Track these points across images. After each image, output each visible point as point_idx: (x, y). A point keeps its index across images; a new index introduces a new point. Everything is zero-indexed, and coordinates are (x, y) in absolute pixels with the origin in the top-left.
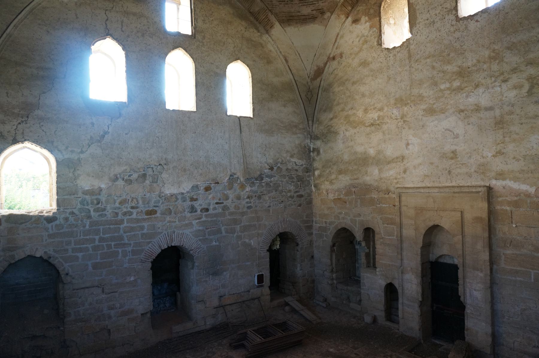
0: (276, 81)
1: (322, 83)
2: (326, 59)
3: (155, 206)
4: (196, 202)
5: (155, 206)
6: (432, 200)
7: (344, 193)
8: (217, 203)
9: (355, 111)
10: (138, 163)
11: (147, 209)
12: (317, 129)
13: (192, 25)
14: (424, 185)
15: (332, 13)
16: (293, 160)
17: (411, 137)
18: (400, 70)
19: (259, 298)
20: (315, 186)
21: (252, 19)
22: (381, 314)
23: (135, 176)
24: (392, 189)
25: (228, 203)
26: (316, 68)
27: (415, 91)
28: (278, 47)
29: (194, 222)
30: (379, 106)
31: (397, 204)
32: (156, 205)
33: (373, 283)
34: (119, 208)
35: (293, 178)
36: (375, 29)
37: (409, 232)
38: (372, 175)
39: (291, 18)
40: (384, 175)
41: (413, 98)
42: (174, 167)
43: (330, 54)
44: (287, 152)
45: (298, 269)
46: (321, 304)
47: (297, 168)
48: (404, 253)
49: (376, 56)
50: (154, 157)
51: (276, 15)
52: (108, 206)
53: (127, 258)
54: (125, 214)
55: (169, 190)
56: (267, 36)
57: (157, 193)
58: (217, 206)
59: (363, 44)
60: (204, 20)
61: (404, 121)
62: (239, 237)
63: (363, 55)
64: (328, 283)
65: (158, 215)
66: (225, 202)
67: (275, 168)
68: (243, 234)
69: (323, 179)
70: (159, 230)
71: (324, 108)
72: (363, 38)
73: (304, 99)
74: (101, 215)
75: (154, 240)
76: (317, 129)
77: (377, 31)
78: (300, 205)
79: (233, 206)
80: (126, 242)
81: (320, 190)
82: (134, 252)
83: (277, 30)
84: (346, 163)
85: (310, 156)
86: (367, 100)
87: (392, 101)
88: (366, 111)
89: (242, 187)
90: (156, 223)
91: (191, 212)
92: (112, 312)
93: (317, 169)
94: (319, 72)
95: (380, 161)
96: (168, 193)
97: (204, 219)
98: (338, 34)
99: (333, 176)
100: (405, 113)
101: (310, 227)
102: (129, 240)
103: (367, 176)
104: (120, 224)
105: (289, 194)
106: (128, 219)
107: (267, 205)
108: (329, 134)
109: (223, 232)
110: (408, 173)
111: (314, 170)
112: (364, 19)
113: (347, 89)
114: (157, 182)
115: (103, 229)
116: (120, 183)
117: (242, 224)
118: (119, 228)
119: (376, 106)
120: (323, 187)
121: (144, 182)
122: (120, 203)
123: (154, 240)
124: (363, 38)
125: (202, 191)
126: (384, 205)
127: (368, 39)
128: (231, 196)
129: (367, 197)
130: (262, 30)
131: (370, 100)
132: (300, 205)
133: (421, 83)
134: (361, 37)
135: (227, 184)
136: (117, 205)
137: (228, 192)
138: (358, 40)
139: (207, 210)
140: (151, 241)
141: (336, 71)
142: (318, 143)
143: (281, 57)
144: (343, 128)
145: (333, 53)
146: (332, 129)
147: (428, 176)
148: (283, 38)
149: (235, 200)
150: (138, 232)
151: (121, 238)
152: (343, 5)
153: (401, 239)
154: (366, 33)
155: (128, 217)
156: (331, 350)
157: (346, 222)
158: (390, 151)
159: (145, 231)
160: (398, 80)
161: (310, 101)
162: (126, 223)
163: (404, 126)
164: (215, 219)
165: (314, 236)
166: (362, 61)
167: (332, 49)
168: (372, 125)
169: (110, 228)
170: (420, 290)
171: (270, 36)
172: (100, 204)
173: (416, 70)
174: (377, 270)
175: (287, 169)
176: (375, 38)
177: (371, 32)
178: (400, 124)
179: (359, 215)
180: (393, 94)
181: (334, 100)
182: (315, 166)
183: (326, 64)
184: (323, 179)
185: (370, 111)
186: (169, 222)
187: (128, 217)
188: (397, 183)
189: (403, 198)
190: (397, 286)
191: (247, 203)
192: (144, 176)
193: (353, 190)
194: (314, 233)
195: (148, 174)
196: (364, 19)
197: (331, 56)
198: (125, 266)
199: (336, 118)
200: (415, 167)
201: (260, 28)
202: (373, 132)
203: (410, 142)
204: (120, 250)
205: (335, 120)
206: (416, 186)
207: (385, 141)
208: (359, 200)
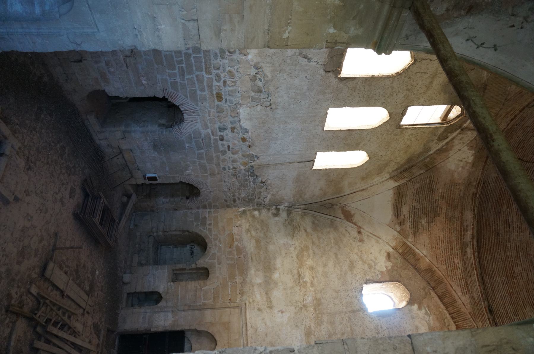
0: (345, 183)
1: (339, 220)
2: (360, 225)
3: (226, 100)
4: (230, 131)
5: (226, 100)
6: (237, 337)
7: (239, 245)
8: (229, 147)
9: (312, 256)
10: (274, 86)
11: (223, 94)
12: (297, 213)
13: (410, 125)
14: (249, 328)
15: (399, 232)
16: (269, 196)
17: (288, 315)
18: (344, 302)
19: (132, 177)
20: (244, 211)
21: (406, 166)
22: (127, 289)
23: (260, 84)
24: (245, 297)
25: (229, 154)
26: (353, 212)
27: (325, 318)
28: (376, 185)
29: (209, 131)
30: (315, 282)
31: (232, 304)
32: (228, 100)
33: (158, 279)
34: (224, 71)
35: (252, 196)
36: (380, 276)
37: (209, 316)
38: (256, 277)
39: (401, 196)
40: (256, 288)
41: (320, 316)
42: (268, 115)
43: (364, 229)
44: (277, 192)
45: (164, 200)
46: (132, 222)
47: (262, 198)
48: (190, 312)
49: (357, 278)
50: (280, 100)
51: (405, 184)
52: (227, 61)
53: (168, 78)
54: (218, 76)
55: (243, 112)
56: (388, 177)
57: (241, 102)
58: (226, 146)
59: (369, 264)
60: (412, 134)
61: (301, 308)
62: (194, 163)
63: (359, 265)
64: (153, 228)
65: (217, 103)
66: (230, 152)
67: (262, 185)
68: (197, 165)
69: (251, 221)
70: (200, 104)
71: (316, 222)
72: (373, 264)
73: (327, 207)
74: (216, 55)
75: (189, 100)
76: (297, 213)
77: (378, 278)
78: (226, 201)
79: (226, 158)
80: (186, 77)
81: (241, 217)
82: (174, 84)
83: (393, 184)
84: (266, 248)
85: (272, 206)
86: (320, 269)
87: (319, 296)
88: (312, 268)
89: (245, 164)
90: (208, 101)
91: (219, 128)
92: (103, 64)
93: (260, 215)
94: (348, 216)
95: (268, 284)
96: (241, 110)
97: (212, 137)
98: (380, 238)
99: (253, 233)
100: (308, 309)
101: (205, 207)
102: (188, 79)
103: (255, 271)
104: (206, 71)
105: (237, 194)
106: (212, 78)
107: (226, 180)
108: (292, 227)
109: (199, 152)
110: (259, 313)
111: (259, 210)
112: (389, 264)
113: (331, 248)
114: (252, 101)
115: (201, 57)
116: (253, 71)
117: (207, 164)
118: (202, 71)
119: (316, 279)
120: (244, 221)
121: (253, 91)
122: (230, 72)
123: (189, 100)
124: (373, 264)
125: (241, 135)
126: (230, 289)
127: (373, 270)
128: (236, 156)
129: (237, 271)
130: (393, 174)
131: (320, 272)
132: (226, 201)
133: (332, 323)
134: (374, 262)
135: (248, 153)
136: (228, 69)
137: (240, 154)
138: (373, 259)
139: (222, 139)
140: (187, 97)
141: (348, 235)
142: (284, 215)
144: (297, 244)
145: (364, 231)
146: (296, 232)
147: (256, 331)
148: (384, 190)
149: (232, 159)
150: (197, 86)
151: (190, 72)
152: (404, 244)
153: (202, 308)
154: (378, 268)
155: (214, 78)
156: (97, 272)
157: (212, 249)
158: (277, 294)
159: (199, 92)
160: (336, 300)
161: (323, 205)
162: (208, 76)
163: (297, 308)
164: (213, 146)
165: (197, 210)
166: (354, 263)
168: (299, 276)
169: (202, 63)
170: (160, 329)
171: (387, 180)
172: (229, 54)
173: (343, 318)
174: (172, 283)
175: (261, 192)
176: (373, 277)
177: (378, 273)
178: (299, 304)
179: (220, 264)
180: (324, 296)
181: (322, 233)
182: (263, 211)
183: (356, 225)
184: (251, 221)
185: (311, 273)
186: (209, 112)
187: (214, 78)
188: (250, 303)
189: (237, 310)
190: (160, 304)
191: (229, 167)
192: (260, 91)
193: (242, 256)
194: (199, 210)
195: (261, 94)
196: (389, 264)
198: (158, 76)
199: (306, 236)
200: (263, 319)
201: (396, 172)
202: (293, 276)
203: (284, 314)
204: (176, 71)
205: (305, 234)
206: (248, 320)
207: (285, 289)
208: (233, 262)
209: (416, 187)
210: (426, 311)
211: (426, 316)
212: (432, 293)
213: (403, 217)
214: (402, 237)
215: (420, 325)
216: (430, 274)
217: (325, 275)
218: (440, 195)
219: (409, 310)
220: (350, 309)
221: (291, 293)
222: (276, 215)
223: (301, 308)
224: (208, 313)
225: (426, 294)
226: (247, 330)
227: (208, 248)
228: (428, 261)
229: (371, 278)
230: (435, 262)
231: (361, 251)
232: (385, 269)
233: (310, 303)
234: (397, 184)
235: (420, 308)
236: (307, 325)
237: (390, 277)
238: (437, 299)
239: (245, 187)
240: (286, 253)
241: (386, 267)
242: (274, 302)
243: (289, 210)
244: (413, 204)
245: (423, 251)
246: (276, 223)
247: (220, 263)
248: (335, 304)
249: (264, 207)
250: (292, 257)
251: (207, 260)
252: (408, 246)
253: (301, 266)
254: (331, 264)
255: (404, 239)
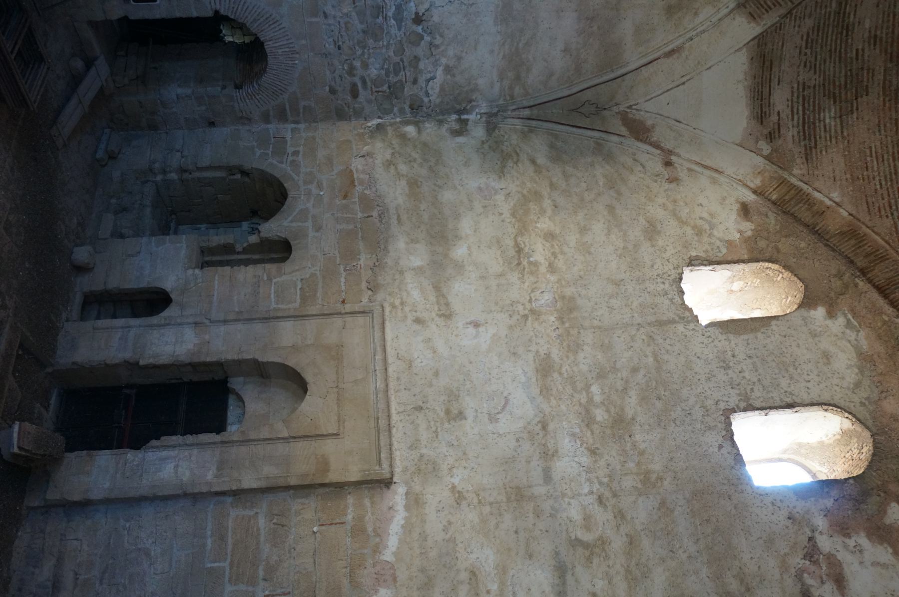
1: (615, 138)
2: (669, 146)
6: (360, 377)
9: (549, 212)
14: (390, 360)
15: (768, 158)
16: (440, 72)
17: (492, 331)
18: (635, 304)
20: (379, 127)
24: (380, 296)
26: (649, 123)
27: (588, 337)
28: (704, 31)
30: (560, 263)
31: (348, 307)
33: (166, 262)
35: (396, 73)
36: (724, 251)
38: (409, 254)
39: (767, 64)
40: (409, 277)
41: (574, 332)
43: (678, 155)
44: (459, 59)
45: (180, 91)
46: (102, 146)
48: (240, 326)
49: (667, 255)
51: (777, 28)
61: (525, 317)
63: (671, 228)
69: (396, 146)
72: (707, 227)
77: (720, 255)
78: (333, 91)
81: (371, 137)
83: (744, 30)
86: (572, 239)
87: (569, 291)
88: (550, 236)
94: (639, 131)
95: (440, 270)
98: (721, 173)
99: (403, 168)
100: (543, 317)
101: (282, 116)
103: (407, 243)
105: (357, 64)
108: (499, 156)
110: (417, 327)
111: (416, 124)
112: (748, 227)
119: (560, 257)
124: (707, 227)
126: (343, 280)
127: (705, 238)
131: (572, 244)
133: (606, 348)
134: (710, 223)
141: (640, 168)
142: (478, 132)
143: (681, 40)
145: (681, 161)
147: (410, 367)
152: (783, 182)
157: (301, 200)
158: (463, 290)
160: (613, 301)
163: (516, 317)
165: (263, 126)
167: (690, 161)
168: (519, 251)
170: (164, 360)
171: (731, 12)
173: (633, 338)
174: (197, 271)
175: (417, 59)
176: (706, 251)
177: (718, 243)
178: (521, 308)
180: (584, 292)
181: (575, 167)
184: (396, 146)
185: (548, 245)
188: (394, 307)
189: (360, 320)
193: (375, 214)
194: (269, 126)
196: (748, 227)
197: (674, 158)
199: (536, 171)
202: (503, 252)
203: (481, 329)
205: (531, 169)
206: (388, 344)
207: (483, 278)
208: (351, 227)
209: (804, 30)
210: (848, 320)
211: (848, 331)
212: (861, 284)
213: (774, 118)
214: (778, 170)
215: (832, 349)
216: (853, 242)
217: (585, 249)
218: (866, 35)
219: (804, 319)
220: (651, 319)
221: (498, 285)
222: (461, 129)
223: (525, 317)
224: (287, 326)
225: (846, 286)
226: (385, 360)
227: (289, 199)
228: (845, 214)
229: (702, 254)
230: (864, 216)
231: (675, 201)
232: (738, 235)
233: (547, 305)
234: (758, 30)
235: (831, 315)
236: (542, 353)
237: (753, 252)
238: (875, 295)
239: (376, 39)
240: (485, 207)
241: (741, 232)
242: (457, 306)
243: (491, 123)
244: (801, 79)
245: (833, 195)
246: (460, 153)
247: (320, 228)
248: (611, 309)
249: (429, 116)
250: (501, 214)
251: (286, 223)
252: (793, 186)
253: (523, 230)
254: (598, 228)
255: (780, 172)
